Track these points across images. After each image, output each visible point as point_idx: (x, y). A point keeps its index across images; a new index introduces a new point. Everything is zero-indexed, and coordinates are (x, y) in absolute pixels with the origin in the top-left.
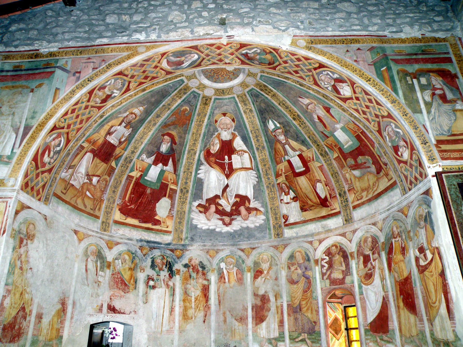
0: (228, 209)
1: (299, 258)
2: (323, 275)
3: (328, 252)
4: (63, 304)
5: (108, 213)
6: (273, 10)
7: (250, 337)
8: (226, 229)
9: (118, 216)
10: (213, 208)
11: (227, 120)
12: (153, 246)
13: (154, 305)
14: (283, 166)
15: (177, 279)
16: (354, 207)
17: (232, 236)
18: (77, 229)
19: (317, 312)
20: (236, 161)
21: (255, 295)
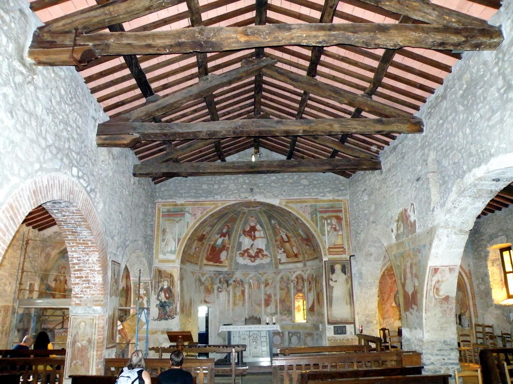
0: (253, 255)
1: (285, 279)
2: (294, 287)
3: (297, 277)
4: (191, 301)
5: (202, 261)
6: (273, 184)
7: (263, 312)
8: (252, 264)
9: (205, 262)
10: (246, 254)
11: (253, 219)
12: (220, 273)
13: (221, 299)
14: (279, 238)
15: (231, 287)
16: (307, 260)
17: (255, 267)
18: (193, 271)
19: (291, 303)
20: (257, 234)
21: (266, 294)
